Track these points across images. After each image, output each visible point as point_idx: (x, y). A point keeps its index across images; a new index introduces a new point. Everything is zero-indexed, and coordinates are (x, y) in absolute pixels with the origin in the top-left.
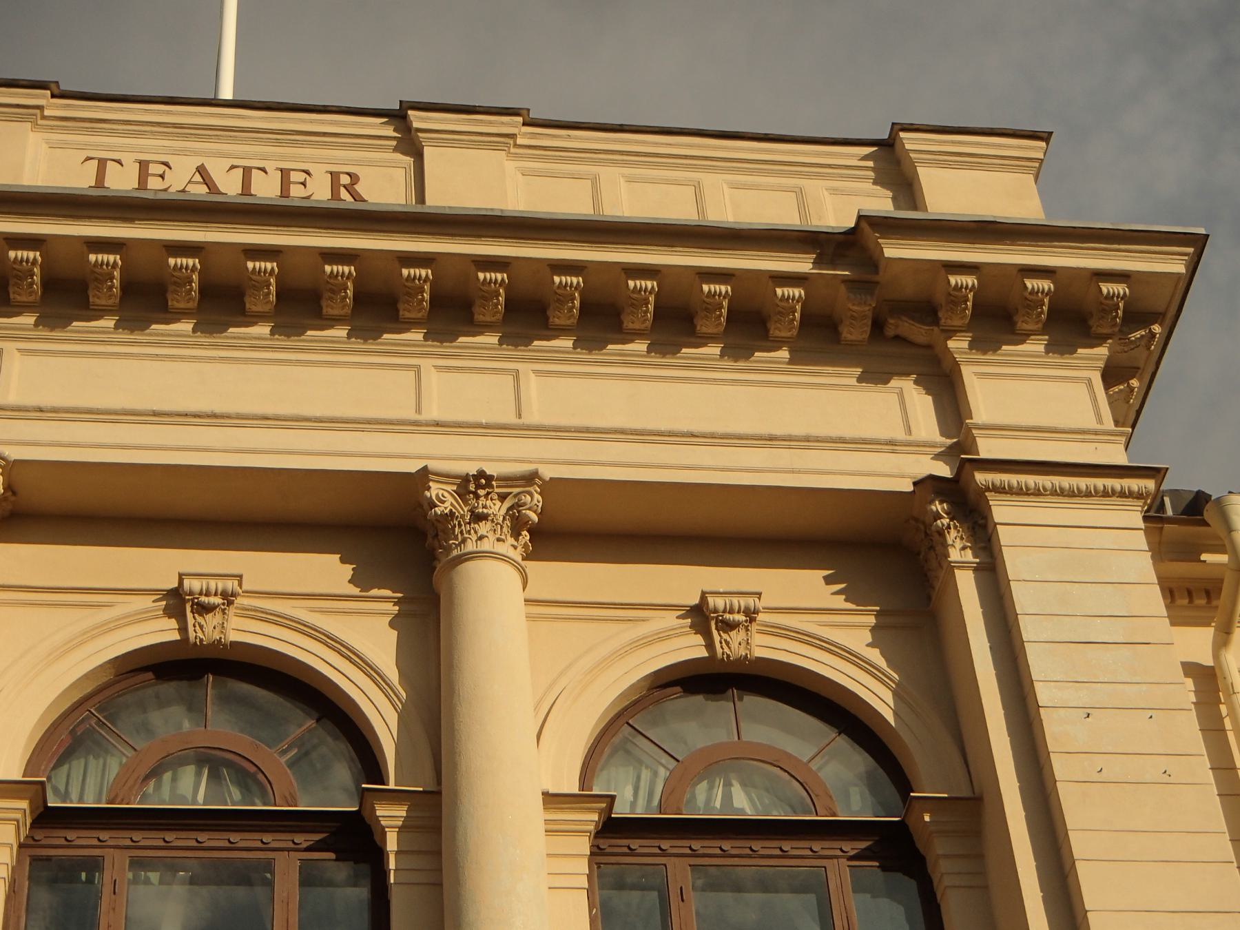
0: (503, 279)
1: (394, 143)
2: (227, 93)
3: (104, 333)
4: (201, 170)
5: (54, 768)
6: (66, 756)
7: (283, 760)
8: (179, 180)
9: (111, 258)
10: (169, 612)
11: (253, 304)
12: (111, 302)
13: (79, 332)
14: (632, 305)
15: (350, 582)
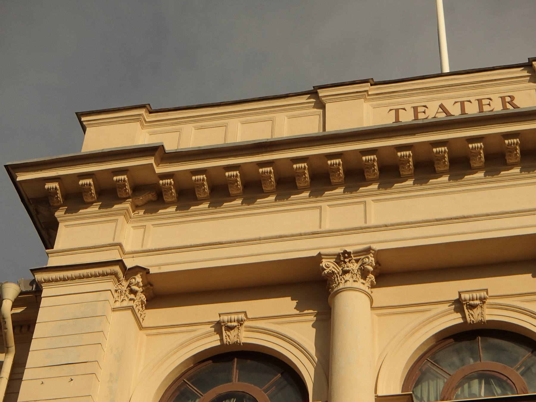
0: (517, 142)
1: (528, 78)
2: (446, 70)
3: (409, 187)
4: (441, 106)
5: (415, 387)
6: (418, 382)
7: (518, 373)
8: (432, 112)
9: (408, 153)
10: (456, 310)
11: (475, 164)
12: (410, 173)
13: (398, 188)
14: (402, 164)
15: (295, 308)
